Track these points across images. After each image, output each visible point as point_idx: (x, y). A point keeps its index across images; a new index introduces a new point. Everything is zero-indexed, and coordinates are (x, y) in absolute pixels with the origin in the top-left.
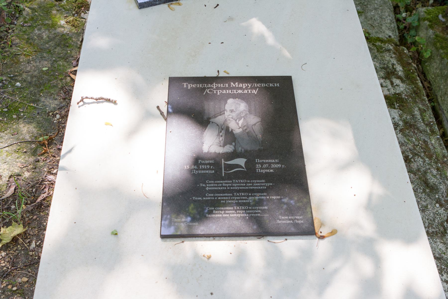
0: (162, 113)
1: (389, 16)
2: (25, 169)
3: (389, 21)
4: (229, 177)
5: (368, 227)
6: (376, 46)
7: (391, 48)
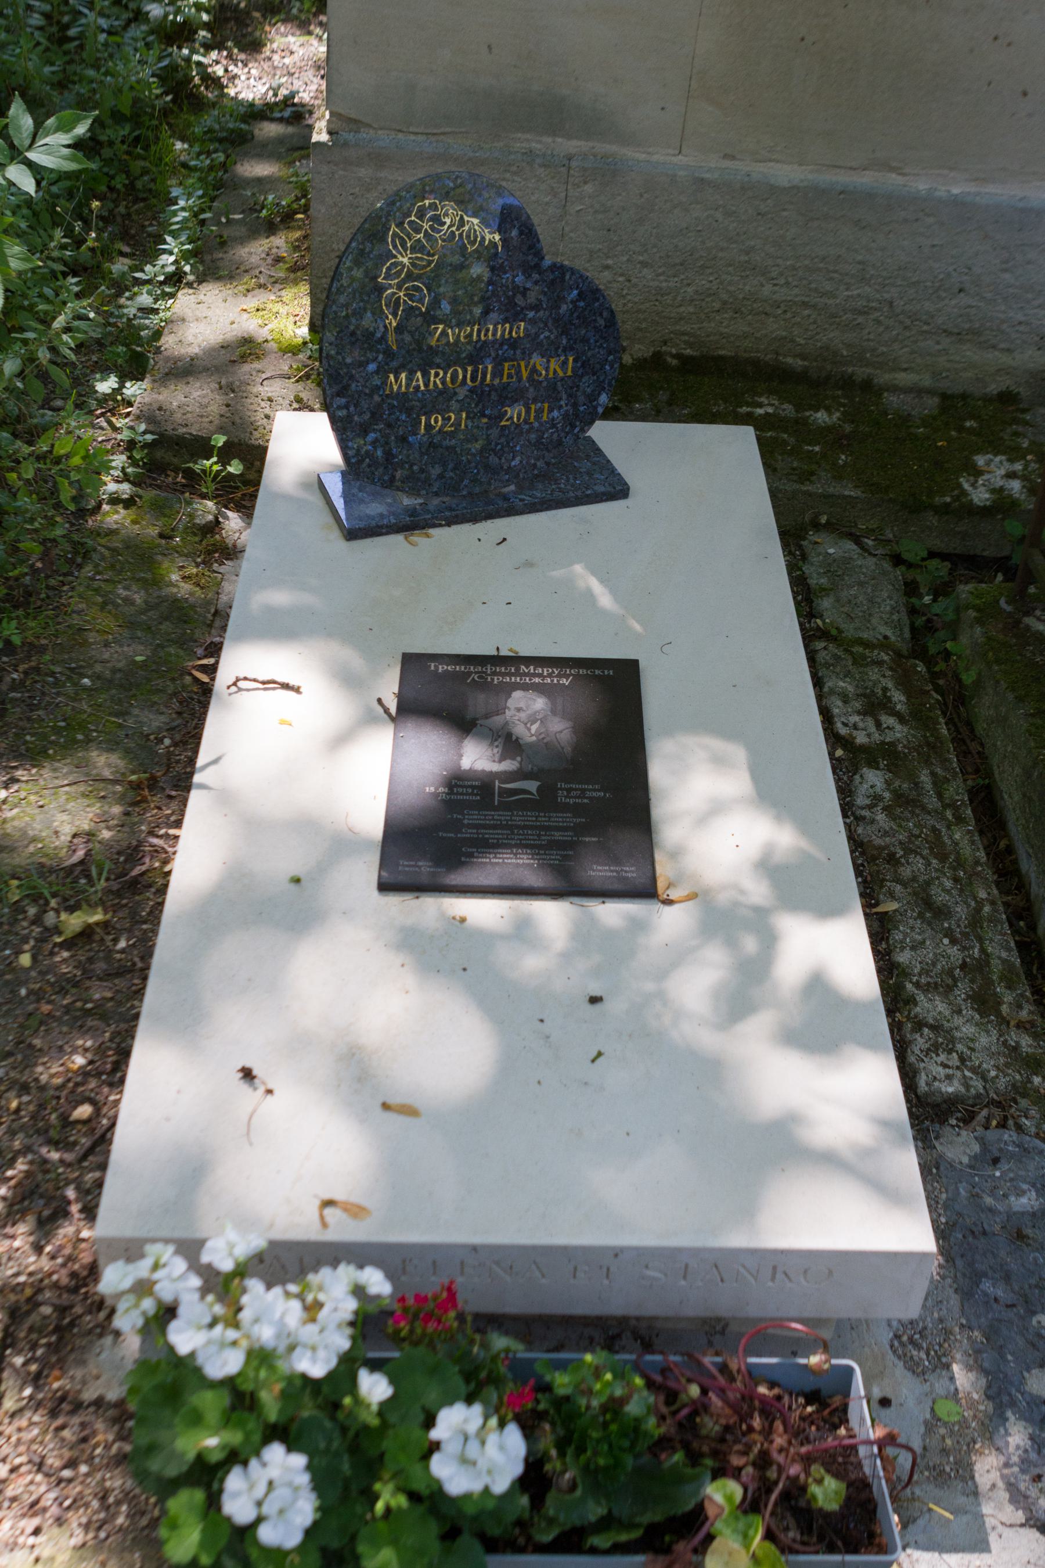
0: (386, 711)
1: (890, 598)
2: (103, 825)
3: (888, 608)
4: (506, 806)
5: (758, 891)
6: (851, 653)
7: (886, 658)
